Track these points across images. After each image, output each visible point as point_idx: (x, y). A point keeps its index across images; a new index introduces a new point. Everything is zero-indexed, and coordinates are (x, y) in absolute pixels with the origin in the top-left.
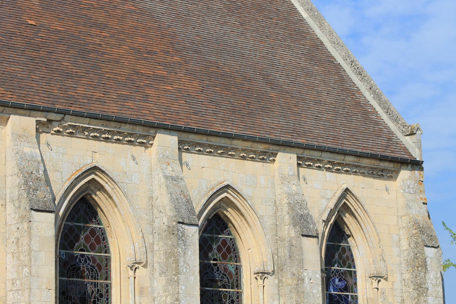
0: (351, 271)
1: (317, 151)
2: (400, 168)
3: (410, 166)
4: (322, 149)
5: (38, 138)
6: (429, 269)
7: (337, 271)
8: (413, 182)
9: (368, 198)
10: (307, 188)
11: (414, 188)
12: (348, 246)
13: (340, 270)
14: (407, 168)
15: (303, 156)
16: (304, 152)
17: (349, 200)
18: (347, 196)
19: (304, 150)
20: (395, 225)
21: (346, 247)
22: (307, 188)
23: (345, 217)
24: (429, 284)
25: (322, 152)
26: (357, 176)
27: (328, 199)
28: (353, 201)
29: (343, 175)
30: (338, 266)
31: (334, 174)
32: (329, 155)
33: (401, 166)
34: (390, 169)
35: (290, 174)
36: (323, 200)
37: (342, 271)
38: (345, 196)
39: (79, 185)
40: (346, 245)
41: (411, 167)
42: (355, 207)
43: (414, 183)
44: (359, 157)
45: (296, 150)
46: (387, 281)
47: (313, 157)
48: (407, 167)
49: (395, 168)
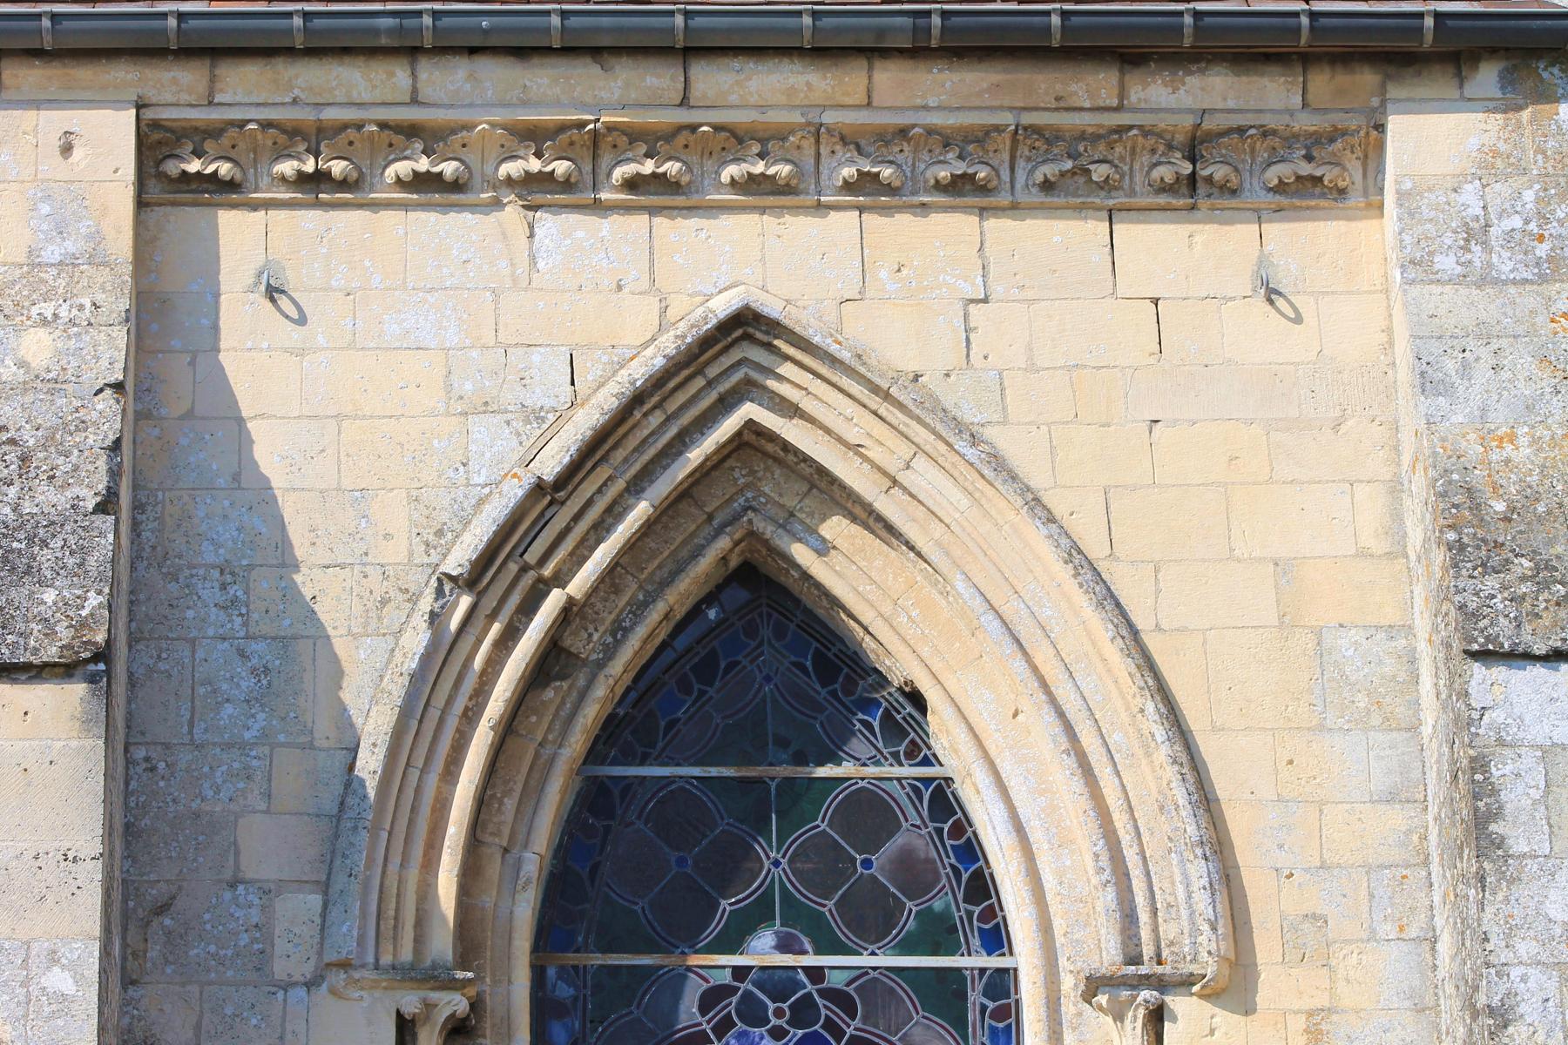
0: (955, 976)
1: (360, 61)
2: (1382, 109)
3: (1487, 77)
4: (376, 32)
5: (244, 489)
6: (1519, 846)
7: (778, 983)
8: (1529, 196)
9: (1032, 368)
10: (301, 353)
11: (1541, 238)
12: (927, 781)
13: (816, 974)
14: (1456, 94)
15: (215, 115)
16: (213, 79)
17: (807, 405)
18: (780, 378)
19: (213, 66)
20: (1363, 554)
21: (901, 794)
22: (301, 353)
23: (824, 549)
24: (1515, 973)
25: (870, 69)
26: (904, 220)
27: (1352, 485)
28: (849, 408)
29: (727, 221)
30: (785, 945)
31: (616, 220)
32: (496, 75)
33: (1383, 86)
34: (1270, 121)
35: (52, 253)
36: (482, 429)
37: (836, 980)
38: (754, 375)
39: (731, 961)
40: (907, 771)
41: (1507, 81)
42: (874, 453)
43: (1538, 200)
44: (863, 63)
45: (123, 74)
46: (1248, 1009)
47: (330, 114)
48: (1461, 86)
49: (1325, 111)
